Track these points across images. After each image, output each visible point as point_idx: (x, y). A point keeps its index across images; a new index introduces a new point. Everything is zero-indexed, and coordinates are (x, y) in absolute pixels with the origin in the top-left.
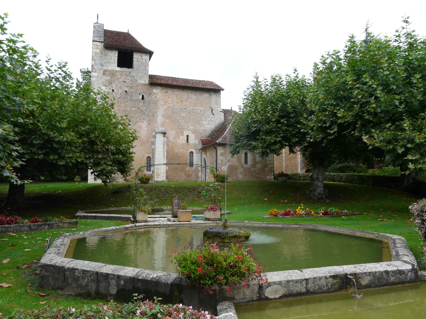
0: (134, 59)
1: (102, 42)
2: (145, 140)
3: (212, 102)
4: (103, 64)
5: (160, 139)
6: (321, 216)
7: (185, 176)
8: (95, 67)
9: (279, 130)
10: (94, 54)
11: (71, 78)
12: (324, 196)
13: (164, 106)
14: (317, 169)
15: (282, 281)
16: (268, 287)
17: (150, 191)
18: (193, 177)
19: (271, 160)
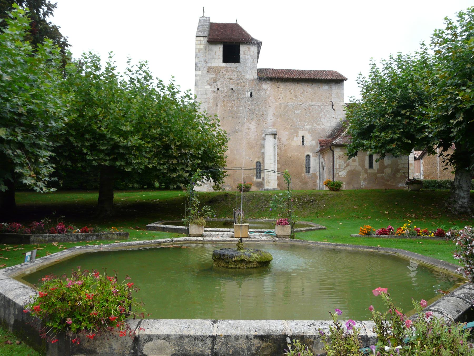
0: (241, 52)
1: (205, 37)
2: (254, 142)
3: (333, 95)
4: (207, 61)
5: (270, 141)
6: (431, 237)
7: (300, 184)
8: (199, 65)
9: (398, 124)
10: (197, 51)
11: (151, 77)
12: (469, 210)
13: (275, 104)
14: (460, 175)
15: (170, 335)
16: (148, 341)
17: (249, 200)
18: (310, 185)
19: (404, 164)
